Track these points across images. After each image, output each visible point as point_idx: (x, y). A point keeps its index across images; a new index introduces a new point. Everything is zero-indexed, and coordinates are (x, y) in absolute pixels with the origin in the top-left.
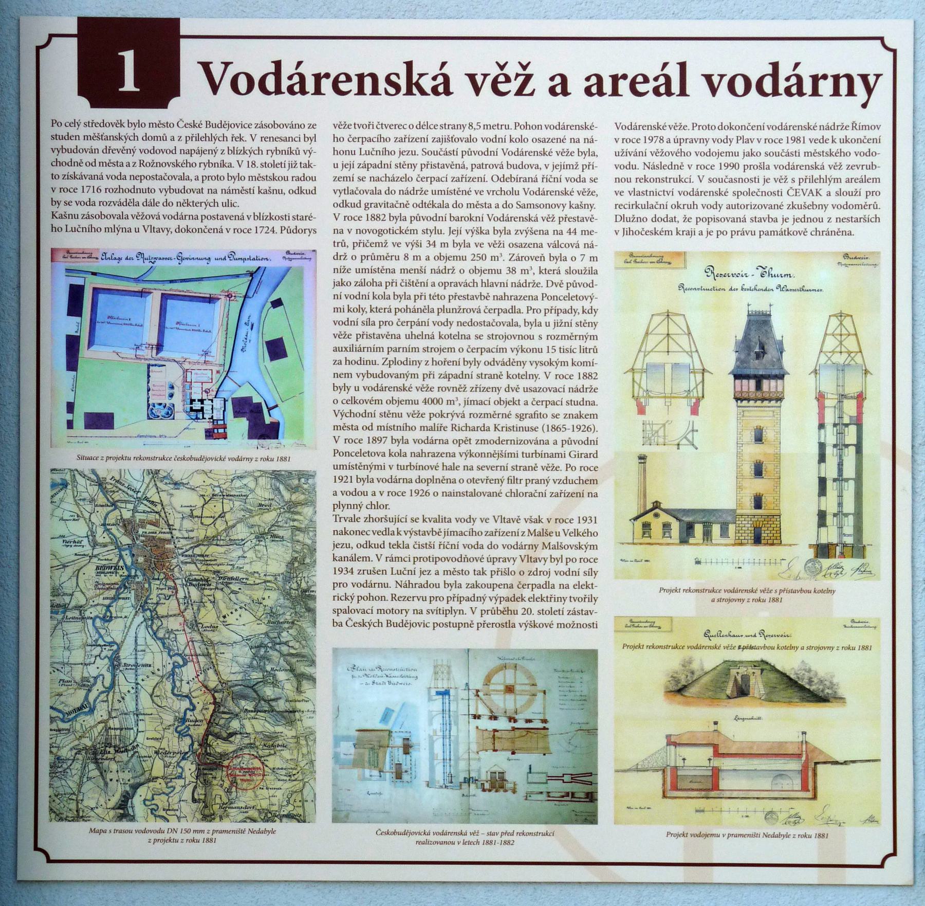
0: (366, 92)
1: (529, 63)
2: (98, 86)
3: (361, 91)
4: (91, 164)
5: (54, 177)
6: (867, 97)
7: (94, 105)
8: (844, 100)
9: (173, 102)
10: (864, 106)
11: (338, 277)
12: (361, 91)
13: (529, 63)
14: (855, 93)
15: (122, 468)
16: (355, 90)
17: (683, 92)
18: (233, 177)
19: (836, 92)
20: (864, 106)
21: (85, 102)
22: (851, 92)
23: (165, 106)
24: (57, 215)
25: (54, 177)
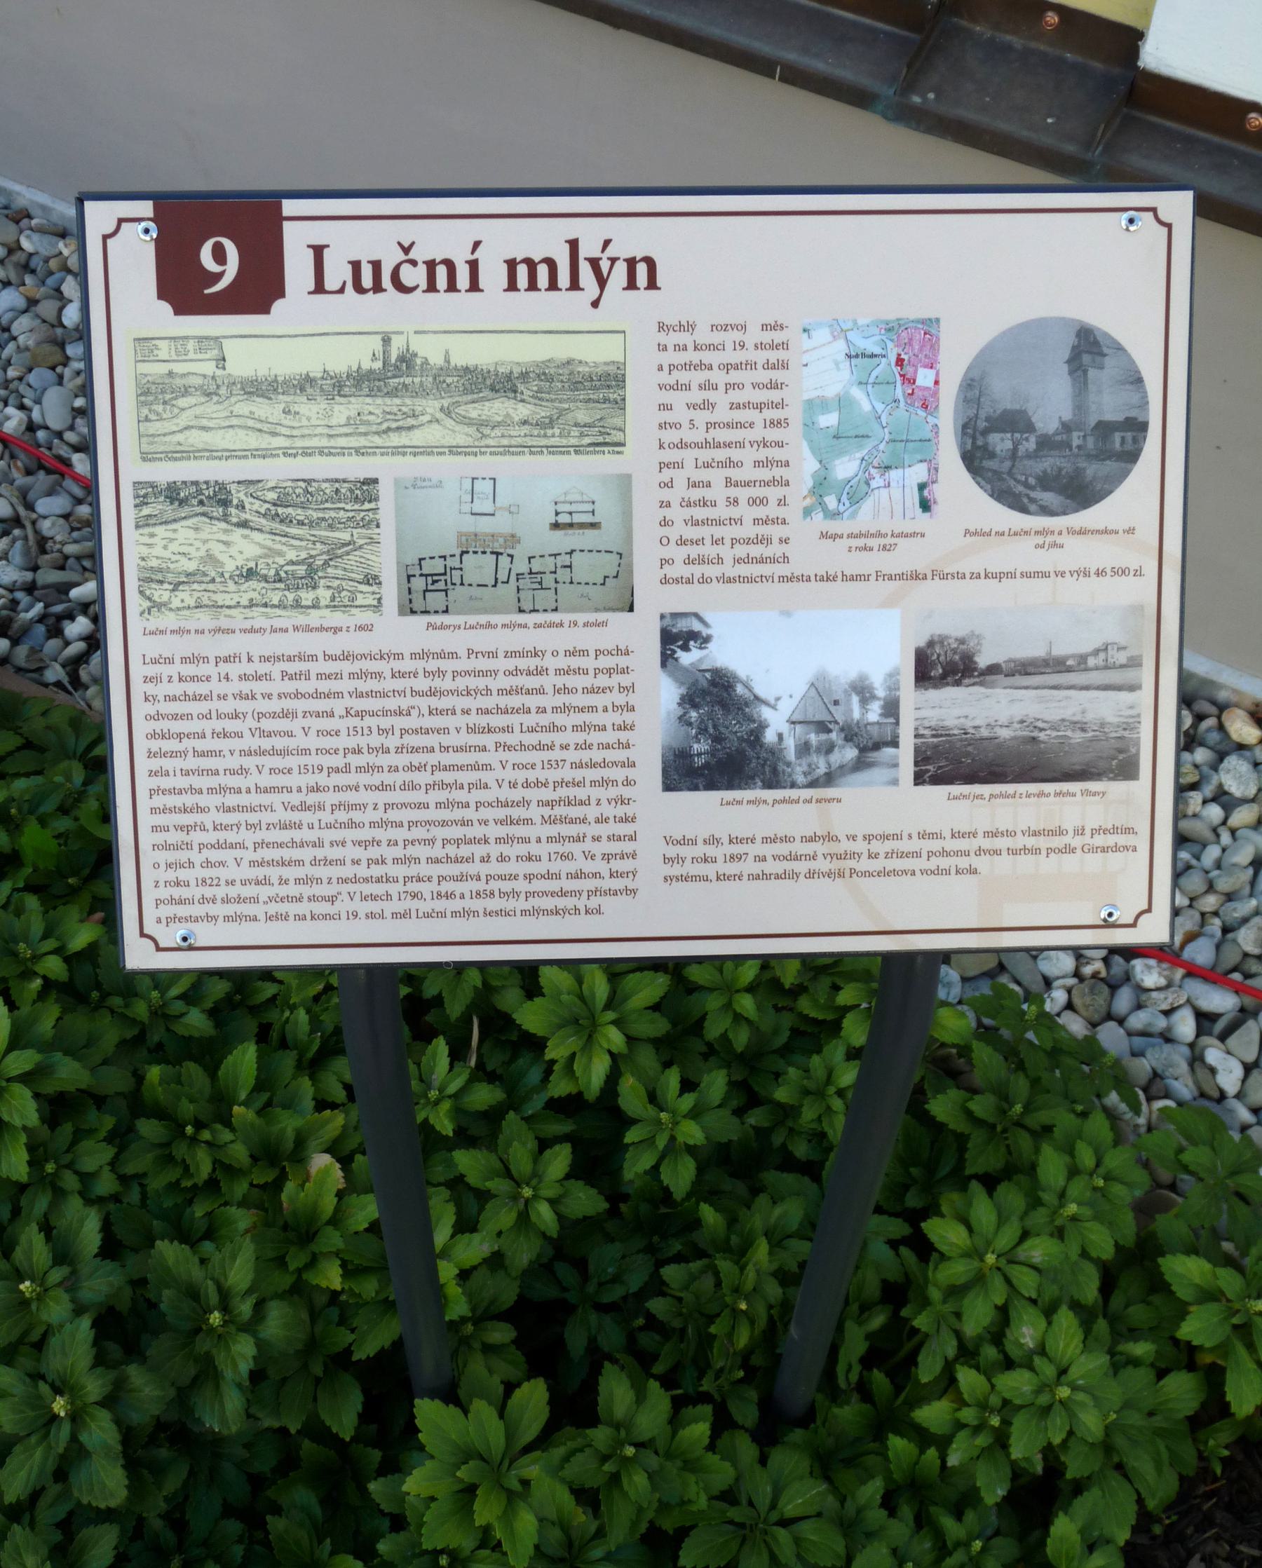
0: (638, 285)
1: (413, 244)
2: (182, 287)
3: (432, 287)
4: (205, 717)
5: (156, 866)
6: (598, 291)
7: (179, 311)
8: (564, 297)
9: (278, 306)
10: (595, 304)
11: (628, 717)
12: (432, 287)
13: (413, 244)
14: (659, 285)
15: (364, 258)
16: (424, 285)
17: (474, 286)
18: (506, 894)
19: (632, 285)
20: (595, 304)
21: (166, 308)
22: (575, 285)
23: (160, 297)
24: (352, 712)
25: (156, 866)
